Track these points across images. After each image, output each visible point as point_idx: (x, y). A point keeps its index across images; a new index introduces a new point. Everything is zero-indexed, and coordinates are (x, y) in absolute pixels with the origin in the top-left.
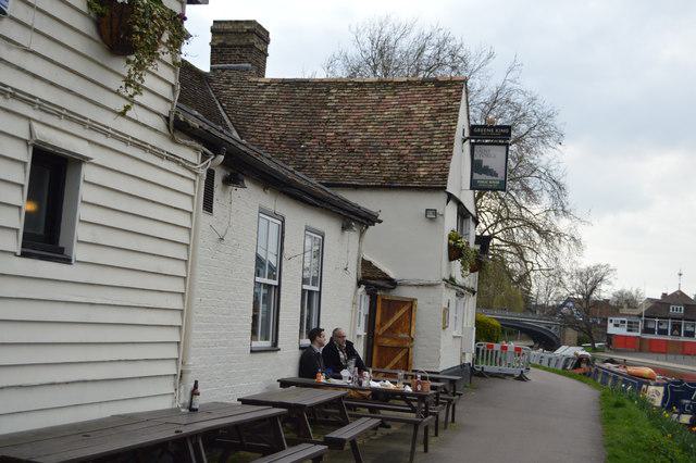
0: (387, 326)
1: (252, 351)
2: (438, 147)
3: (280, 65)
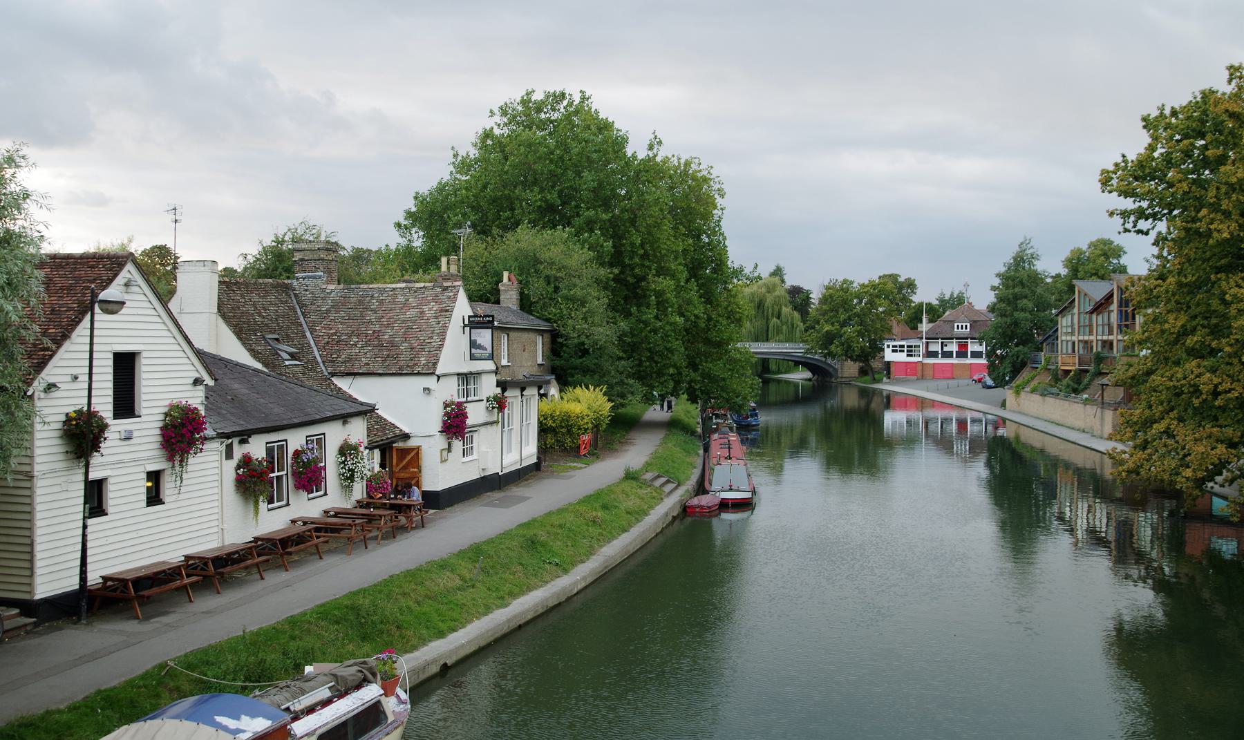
0: (401, 466)
1: (269, 510)
2: (436, 341)
3: (414, 209)
